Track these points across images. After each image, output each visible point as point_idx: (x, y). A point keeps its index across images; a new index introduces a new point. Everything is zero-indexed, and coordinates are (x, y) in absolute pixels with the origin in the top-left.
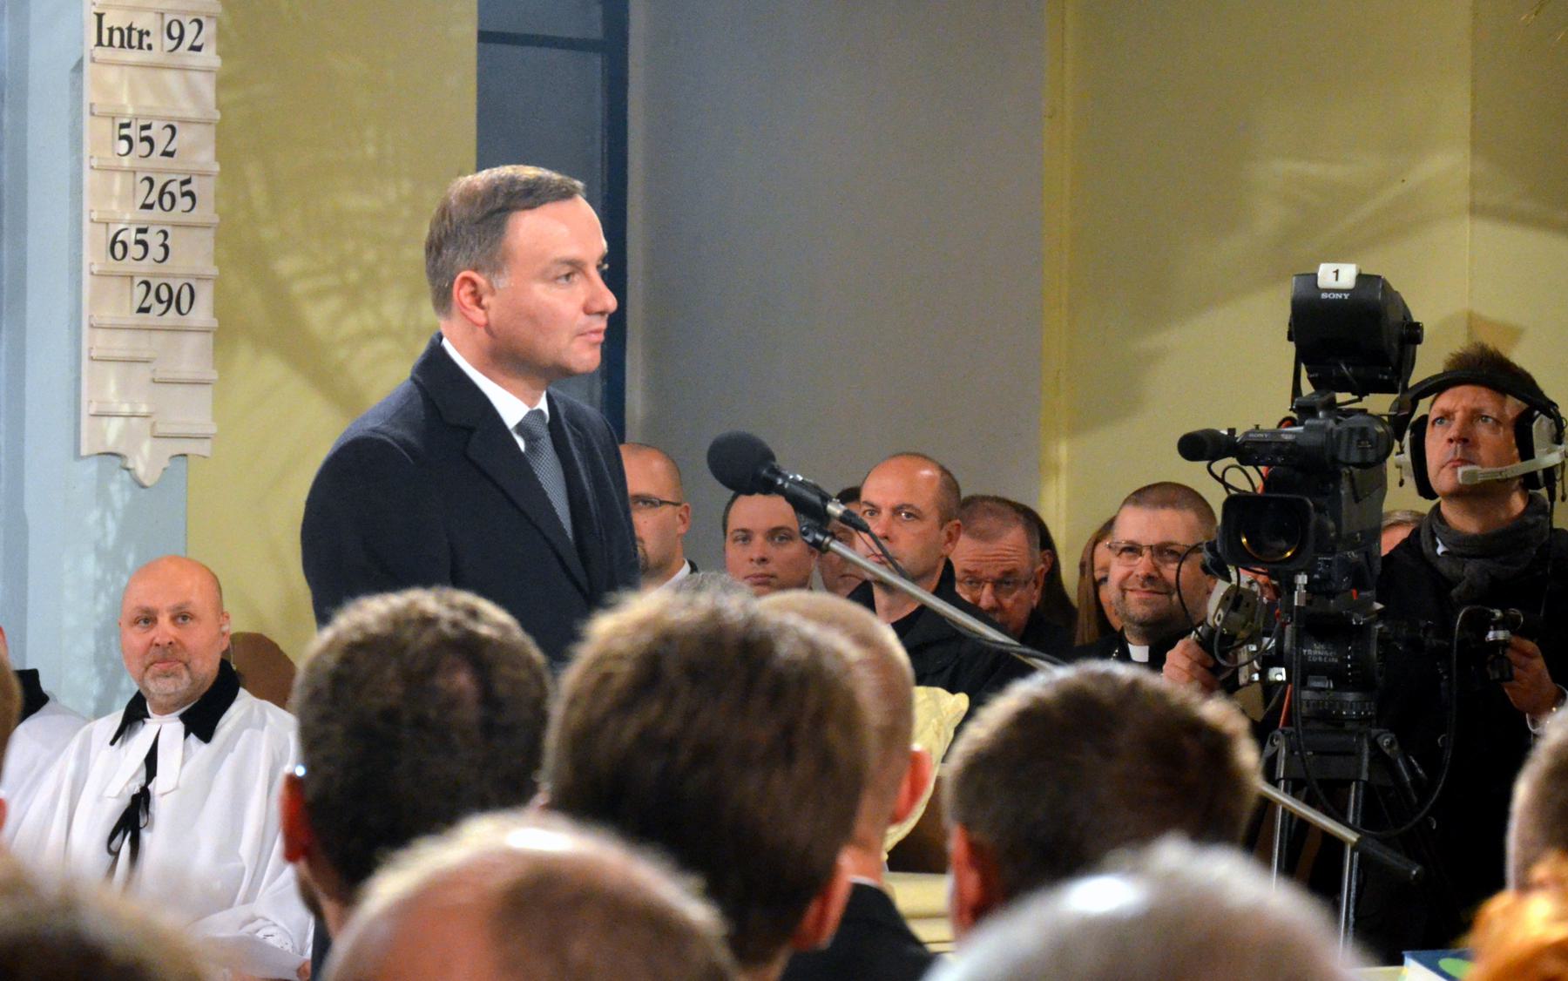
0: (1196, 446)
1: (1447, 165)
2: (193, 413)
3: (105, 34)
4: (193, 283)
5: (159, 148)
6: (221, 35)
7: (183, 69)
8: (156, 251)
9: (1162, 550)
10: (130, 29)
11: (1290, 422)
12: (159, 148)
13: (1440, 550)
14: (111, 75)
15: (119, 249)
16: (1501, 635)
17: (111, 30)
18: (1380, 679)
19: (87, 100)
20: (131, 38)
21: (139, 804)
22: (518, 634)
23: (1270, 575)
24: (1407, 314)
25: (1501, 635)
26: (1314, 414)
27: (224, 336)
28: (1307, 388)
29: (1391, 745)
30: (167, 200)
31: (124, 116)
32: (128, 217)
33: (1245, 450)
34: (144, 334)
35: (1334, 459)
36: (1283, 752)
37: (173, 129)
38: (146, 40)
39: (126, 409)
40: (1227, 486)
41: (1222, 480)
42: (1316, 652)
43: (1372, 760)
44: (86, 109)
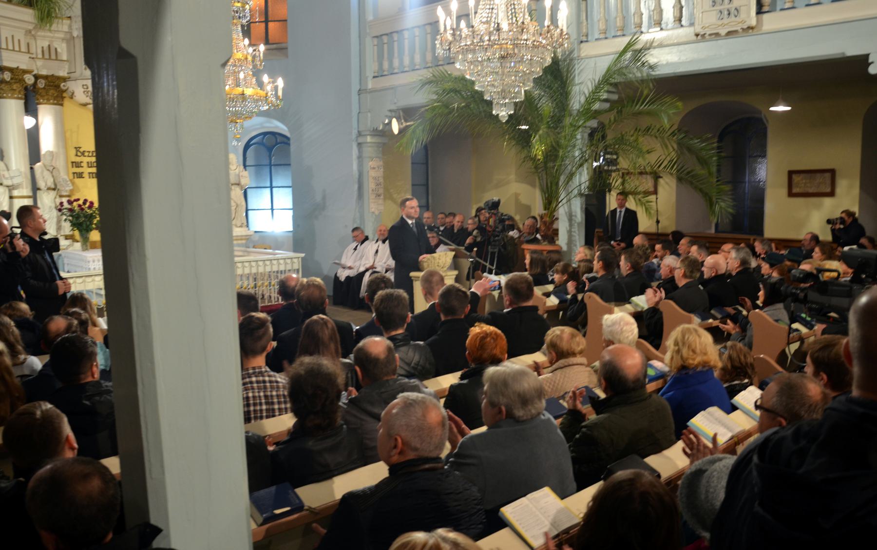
1: (513, 177)
2: (382, 208)
20: (374, 168)
21: (377, 252)
22: (54, 408)
27: (385, 199)
34: (263, 35)
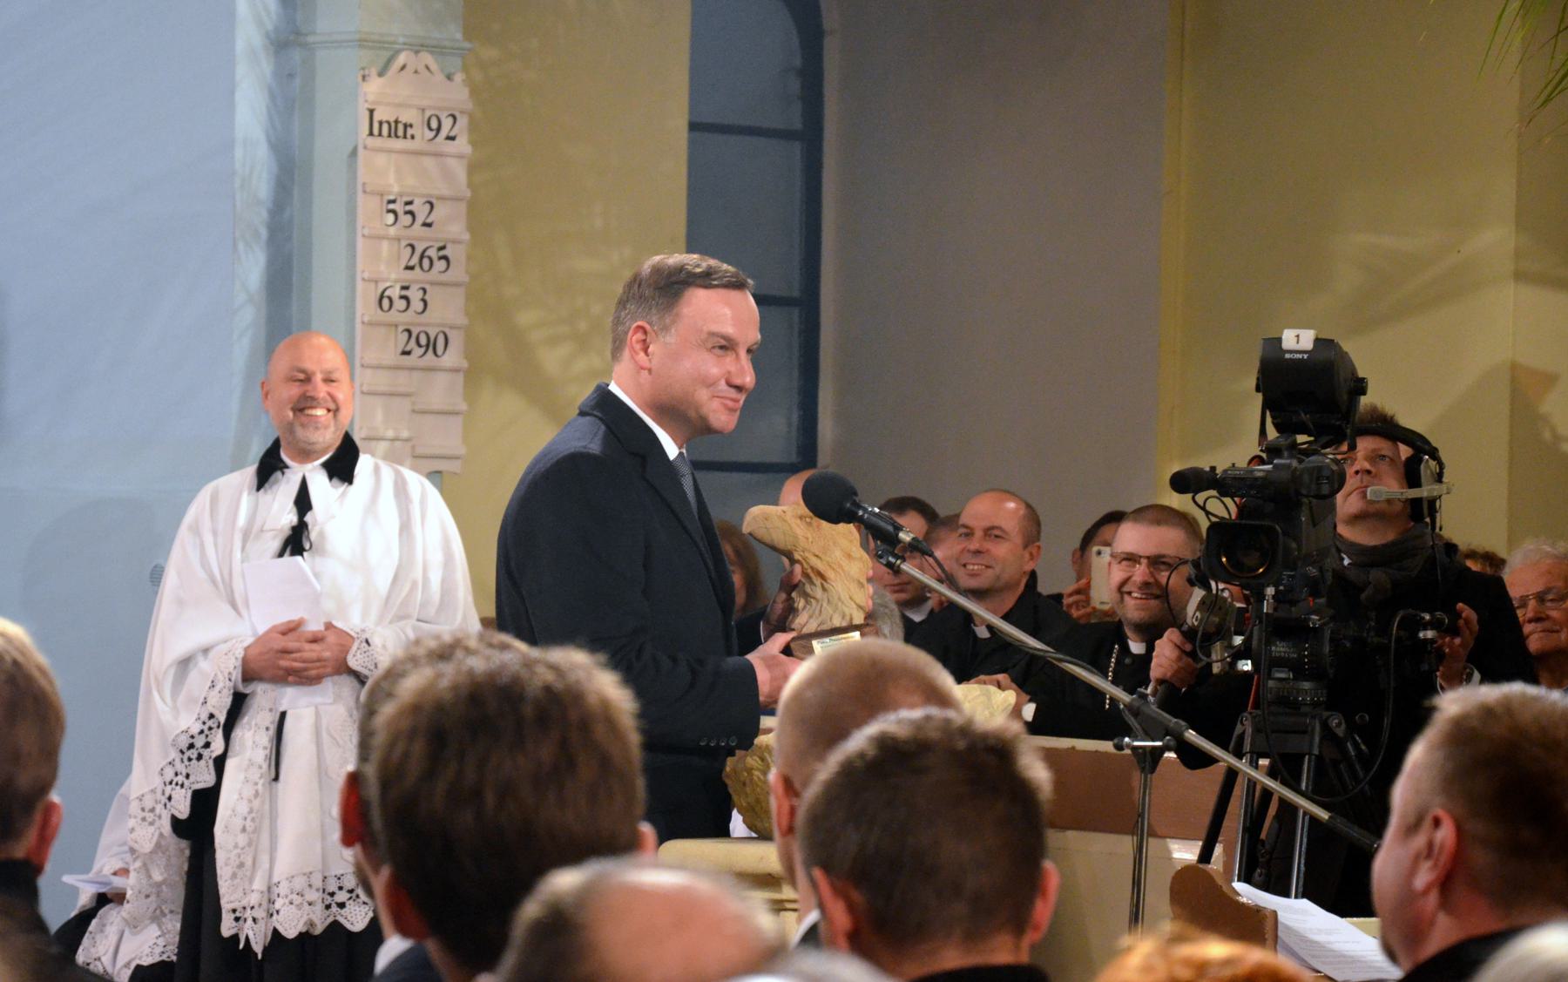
0: (1184, 482)
1: (1496, 238)
3: (376, 126)
4: (447, 330)
5: (420, 220)
6: (473, 127)
7: (437, 154)
8: (417, 305)
9: (1156, 561)
10: (397, 122)
11: (1257, 459)
12: (420, 220)
13: (1346, 562)
14: (381, 160)
15: (386, 303)
16: (1430, 634)
17: (381, 123)
18: (1331, 671)
19: (360, 181)
20: (398, 129)
23: (1243, 587)
24: (1354, 371)
25: (1430, 634)
26: (1280, 456)
27: (473, 375)
28: (1272, 433)
29: (1339, 725)
30: (426, 262)
31: (389, 193)
32: (393, 276)
33: (1223, 484)
35: (1298, 493)
36: (1249, 731)
37: (432, 205)
38: (410, 132)
39: (390, 434)
40: (1208, 513)
41: (1203, 508)
42: (1280, 649)
43: (1322, 739)
44: (360, 188)
